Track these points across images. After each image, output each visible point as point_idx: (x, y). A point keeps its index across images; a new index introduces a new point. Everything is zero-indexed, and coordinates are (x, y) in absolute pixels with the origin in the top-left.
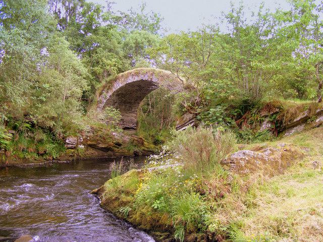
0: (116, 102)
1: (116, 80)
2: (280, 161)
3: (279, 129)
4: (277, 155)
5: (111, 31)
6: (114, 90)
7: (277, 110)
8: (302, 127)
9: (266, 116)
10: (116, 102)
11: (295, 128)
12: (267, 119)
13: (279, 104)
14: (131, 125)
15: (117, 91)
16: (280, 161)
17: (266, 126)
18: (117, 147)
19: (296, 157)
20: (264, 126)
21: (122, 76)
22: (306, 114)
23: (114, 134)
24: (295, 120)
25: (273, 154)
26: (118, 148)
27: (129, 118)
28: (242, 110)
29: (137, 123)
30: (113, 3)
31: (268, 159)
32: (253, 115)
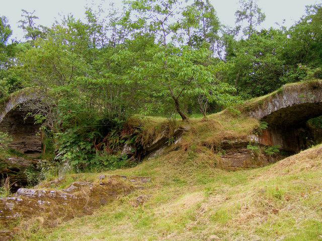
0: (13, 124)
1: (7, 101)
2: (88, 198)
3: (141, 153)
4: (85, 191)
5: (15, 47)
6: (7, 111)
7: (136, 131)
8: (161, 151)
9: (126, 139)
10: (13, 124)
11: (158, 151)
12: (127, 142)
13: (138, 124)
14: (35, 148)
15: (9, 113)
16: (88, 198)
17: (127, 149)
18: (14, 173)
19: (119, 191)
20: (124, 150)
21: (14, 96)
22: (163, 135)
23: (10, 159)
24: (153, 143)
25: (78, 190)
26: (16, 174)
27: (32, 140)
28: (100, 131)
29: (42, 146)
30: (35, 17)
31: (68, 197)
32: (113, 139)
